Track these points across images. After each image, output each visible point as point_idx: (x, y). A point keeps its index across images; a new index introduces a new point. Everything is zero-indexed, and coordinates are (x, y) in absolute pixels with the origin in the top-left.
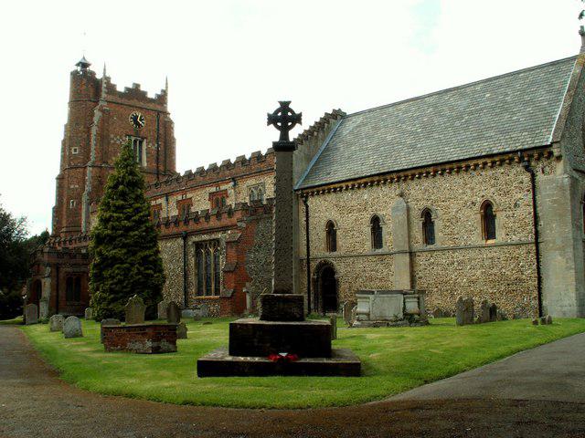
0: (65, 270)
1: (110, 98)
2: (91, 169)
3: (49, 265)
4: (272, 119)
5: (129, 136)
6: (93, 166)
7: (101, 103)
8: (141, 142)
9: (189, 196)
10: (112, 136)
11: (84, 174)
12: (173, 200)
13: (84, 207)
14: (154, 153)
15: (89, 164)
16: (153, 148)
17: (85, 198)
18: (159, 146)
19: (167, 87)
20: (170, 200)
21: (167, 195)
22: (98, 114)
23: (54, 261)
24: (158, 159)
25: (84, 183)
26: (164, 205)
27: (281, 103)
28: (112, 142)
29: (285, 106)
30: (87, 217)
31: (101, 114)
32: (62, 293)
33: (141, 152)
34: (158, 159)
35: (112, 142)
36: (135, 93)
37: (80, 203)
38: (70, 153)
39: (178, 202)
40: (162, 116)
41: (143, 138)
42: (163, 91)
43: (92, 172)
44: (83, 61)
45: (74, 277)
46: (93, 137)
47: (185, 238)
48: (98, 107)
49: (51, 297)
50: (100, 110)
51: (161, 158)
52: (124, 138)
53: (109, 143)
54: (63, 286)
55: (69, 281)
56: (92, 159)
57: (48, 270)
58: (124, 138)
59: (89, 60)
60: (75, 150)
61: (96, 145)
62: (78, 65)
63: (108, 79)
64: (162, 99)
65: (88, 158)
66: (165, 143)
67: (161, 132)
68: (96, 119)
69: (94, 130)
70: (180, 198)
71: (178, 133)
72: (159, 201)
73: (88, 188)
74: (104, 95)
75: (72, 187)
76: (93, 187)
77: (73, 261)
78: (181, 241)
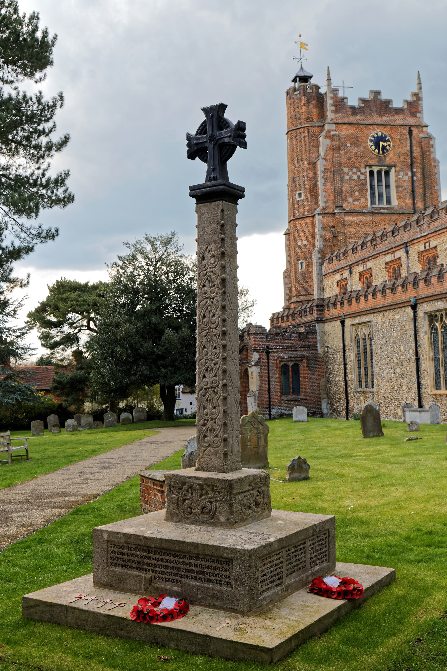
0: (279, 354)
1: (340, 118)
2: (321, 217)
3: (255, 350)
4: (195, 150)
5: (370, 166)
6: (323, 214)
7: (327, 127)
8: (387, 174)
9: (433, 243)
10: (346, 170)
11: (313, 226)
12: (414, 250)
13: (315, 268)
14: (407, 185)
15: (318, 211)
16: (406, 178)
17: (315, 257)
18: (413, 174)
19: (420, 88)
20: (354, 270)
21: (406, 245)
22: (324, 143)
23: (262, 345)
24: (413, 191)
25: (314, 237)
26: (404, 259)
27: (206, 111)
28: (347, 177)
29: (216, 115)
30: (321, 282)
31: (328, 142)
32: (275, 386)
33: (388, 186)
34: (413, 191)
35: (347, 177)
36: (376, 104)
37: (310, 264)
38: (294, 199)
39: (420, 253)
40: (415, 131)
41: (390, 167)
42: (416, 95)
43: (322, 222)
44: (302, 74)
45: (291, 364)
46: (320, 175)
47: (414, 307)
48: (324, 133)
49: (260, 390)
50: (328, 137)
51: (419, 190)
52: (363, 170)
53: (342, 179)
54: (275, 375)
55: (284, 369)
56: (321, 204)
57: (255, 356)
58: (363, 170)
59: (308, 71)
60: (300, 195)
61: (325, 185)
62: (294, 80)
63: (335, 91)
64: (414, 106)
65: (317, 203)
66: (423, 169)
67: (417, 153)
68: (322, 151)
69: (320, 165)
70: (422, 248)
71: (439, 152)
72: (398, 254)
73: (318, 244)
74: (330, 115)
75: (299, 243)
76: (325, 241)
77: (287, 343)
78: (409, 311)
